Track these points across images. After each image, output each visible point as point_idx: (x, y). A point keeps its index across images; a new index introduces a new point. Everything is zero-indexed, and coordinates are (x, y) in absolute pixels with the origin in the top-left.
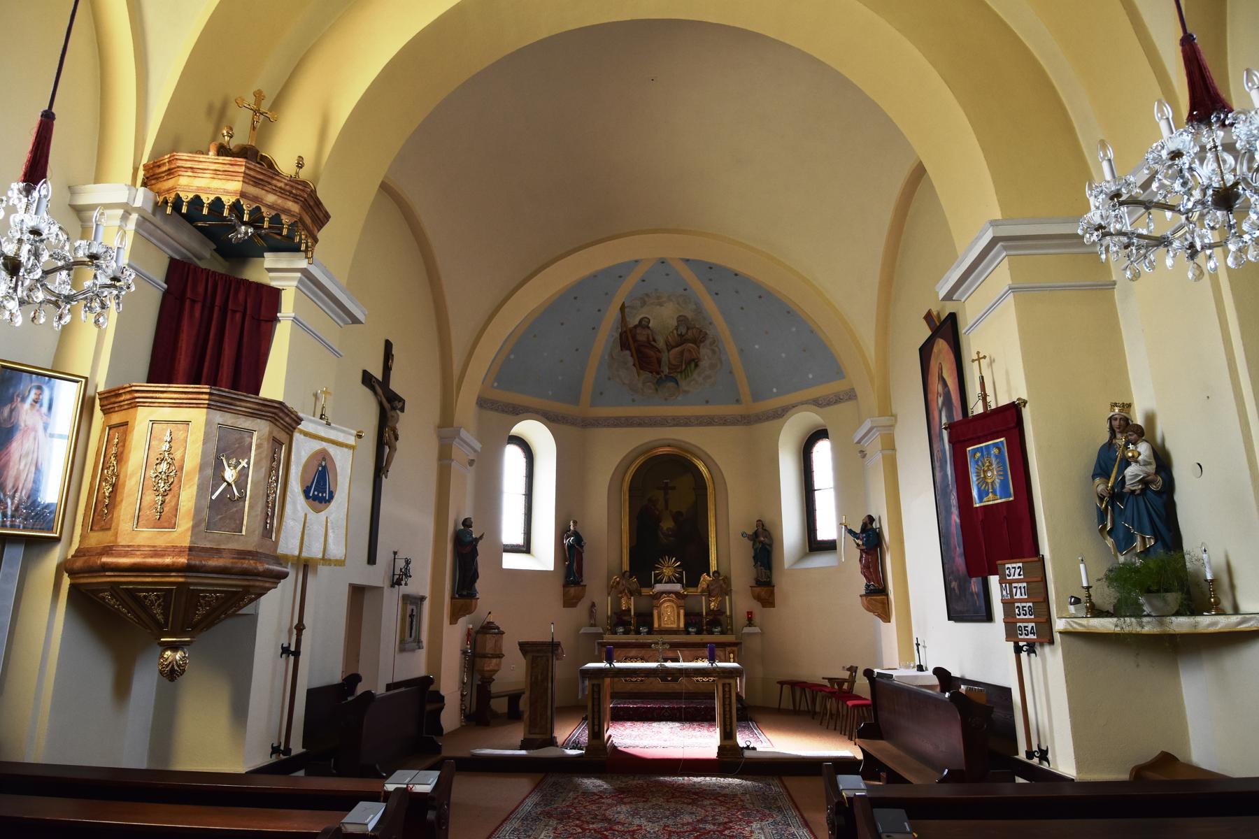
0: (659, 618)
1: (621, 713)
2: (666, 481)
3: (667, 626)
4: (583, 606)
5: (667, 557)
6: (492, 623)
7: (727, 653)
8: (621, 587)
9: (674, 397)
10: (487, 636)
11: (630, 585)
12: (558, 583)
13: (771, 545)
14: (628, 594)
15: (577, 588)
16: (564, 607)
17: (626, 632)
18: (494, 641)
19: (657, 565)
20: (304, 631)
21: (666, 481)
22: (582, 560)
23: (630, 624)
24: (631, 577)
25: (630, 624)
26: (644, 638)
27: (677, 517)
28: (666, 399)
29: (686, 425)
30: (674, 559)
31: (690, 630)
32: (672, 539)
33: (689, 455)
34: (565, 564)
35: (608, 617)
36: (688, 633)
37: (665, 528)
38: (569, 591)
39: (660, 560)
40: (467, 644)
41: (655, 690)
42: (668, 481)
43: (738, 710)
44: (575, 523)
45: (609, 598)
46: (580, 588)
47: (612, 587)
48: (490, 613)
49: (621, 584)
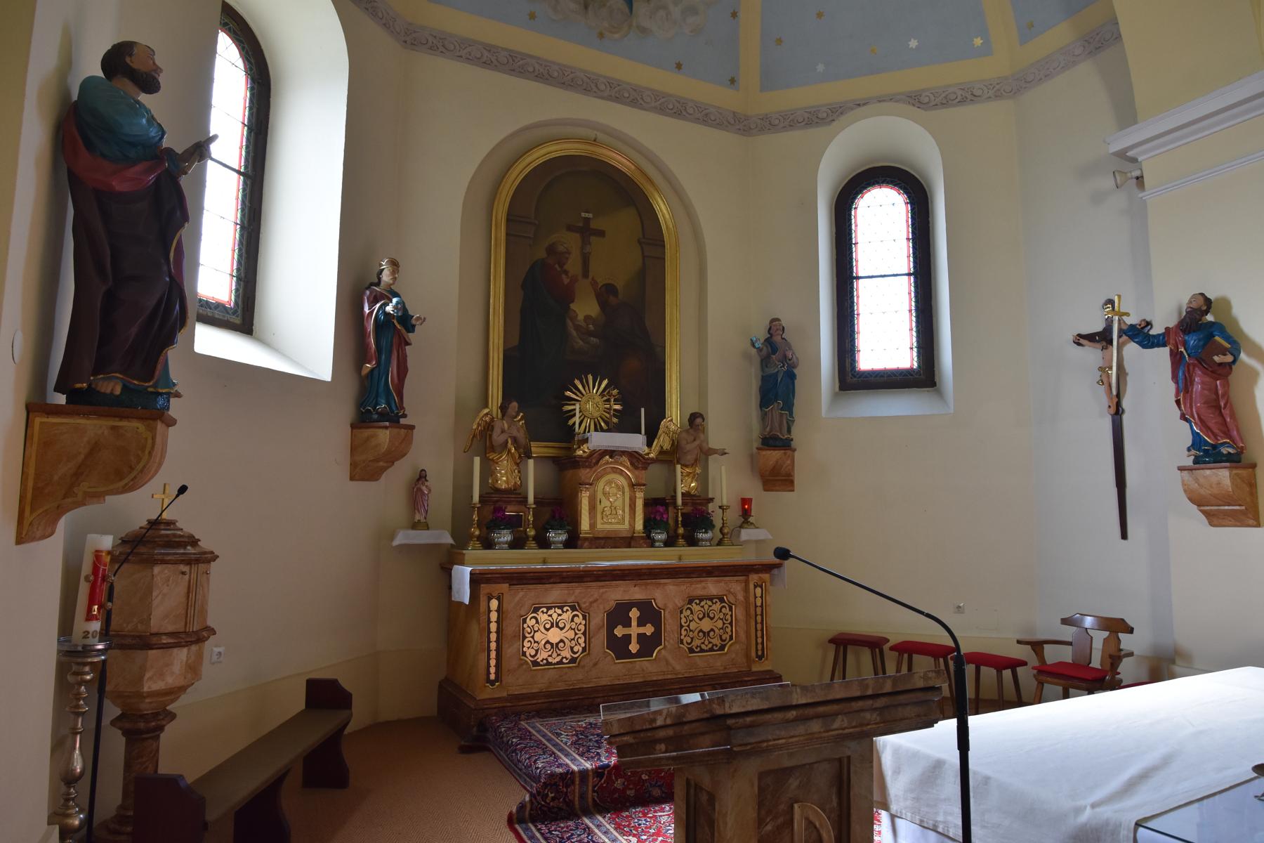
0: (593, 508)
1: (619, 784)
2: (587, 215)
3: (608, 527)
4: (397, 477)
5: (590, 377)
6: (170, 523)
7: (752, 586)
9: (617, 36)
10: (157, 569)
12: (344, 411)
16: (352, 479)
17: (517, 544)
18: (182, 589)
19: (568, 393)
20: (1190, 443)
21: (587, 215)
26: (560, 559)
27: (605, 294)
28: (601, 36)
30: (605, 382)
31: (551, 534)
36: (652, 543)
37: (581, 317)
38: (368, 439)
39: (577, 382)
40: (89, 617)
41: (605, 681)
42: (590, 216)
44: (394, 264)
48: (183, 490)
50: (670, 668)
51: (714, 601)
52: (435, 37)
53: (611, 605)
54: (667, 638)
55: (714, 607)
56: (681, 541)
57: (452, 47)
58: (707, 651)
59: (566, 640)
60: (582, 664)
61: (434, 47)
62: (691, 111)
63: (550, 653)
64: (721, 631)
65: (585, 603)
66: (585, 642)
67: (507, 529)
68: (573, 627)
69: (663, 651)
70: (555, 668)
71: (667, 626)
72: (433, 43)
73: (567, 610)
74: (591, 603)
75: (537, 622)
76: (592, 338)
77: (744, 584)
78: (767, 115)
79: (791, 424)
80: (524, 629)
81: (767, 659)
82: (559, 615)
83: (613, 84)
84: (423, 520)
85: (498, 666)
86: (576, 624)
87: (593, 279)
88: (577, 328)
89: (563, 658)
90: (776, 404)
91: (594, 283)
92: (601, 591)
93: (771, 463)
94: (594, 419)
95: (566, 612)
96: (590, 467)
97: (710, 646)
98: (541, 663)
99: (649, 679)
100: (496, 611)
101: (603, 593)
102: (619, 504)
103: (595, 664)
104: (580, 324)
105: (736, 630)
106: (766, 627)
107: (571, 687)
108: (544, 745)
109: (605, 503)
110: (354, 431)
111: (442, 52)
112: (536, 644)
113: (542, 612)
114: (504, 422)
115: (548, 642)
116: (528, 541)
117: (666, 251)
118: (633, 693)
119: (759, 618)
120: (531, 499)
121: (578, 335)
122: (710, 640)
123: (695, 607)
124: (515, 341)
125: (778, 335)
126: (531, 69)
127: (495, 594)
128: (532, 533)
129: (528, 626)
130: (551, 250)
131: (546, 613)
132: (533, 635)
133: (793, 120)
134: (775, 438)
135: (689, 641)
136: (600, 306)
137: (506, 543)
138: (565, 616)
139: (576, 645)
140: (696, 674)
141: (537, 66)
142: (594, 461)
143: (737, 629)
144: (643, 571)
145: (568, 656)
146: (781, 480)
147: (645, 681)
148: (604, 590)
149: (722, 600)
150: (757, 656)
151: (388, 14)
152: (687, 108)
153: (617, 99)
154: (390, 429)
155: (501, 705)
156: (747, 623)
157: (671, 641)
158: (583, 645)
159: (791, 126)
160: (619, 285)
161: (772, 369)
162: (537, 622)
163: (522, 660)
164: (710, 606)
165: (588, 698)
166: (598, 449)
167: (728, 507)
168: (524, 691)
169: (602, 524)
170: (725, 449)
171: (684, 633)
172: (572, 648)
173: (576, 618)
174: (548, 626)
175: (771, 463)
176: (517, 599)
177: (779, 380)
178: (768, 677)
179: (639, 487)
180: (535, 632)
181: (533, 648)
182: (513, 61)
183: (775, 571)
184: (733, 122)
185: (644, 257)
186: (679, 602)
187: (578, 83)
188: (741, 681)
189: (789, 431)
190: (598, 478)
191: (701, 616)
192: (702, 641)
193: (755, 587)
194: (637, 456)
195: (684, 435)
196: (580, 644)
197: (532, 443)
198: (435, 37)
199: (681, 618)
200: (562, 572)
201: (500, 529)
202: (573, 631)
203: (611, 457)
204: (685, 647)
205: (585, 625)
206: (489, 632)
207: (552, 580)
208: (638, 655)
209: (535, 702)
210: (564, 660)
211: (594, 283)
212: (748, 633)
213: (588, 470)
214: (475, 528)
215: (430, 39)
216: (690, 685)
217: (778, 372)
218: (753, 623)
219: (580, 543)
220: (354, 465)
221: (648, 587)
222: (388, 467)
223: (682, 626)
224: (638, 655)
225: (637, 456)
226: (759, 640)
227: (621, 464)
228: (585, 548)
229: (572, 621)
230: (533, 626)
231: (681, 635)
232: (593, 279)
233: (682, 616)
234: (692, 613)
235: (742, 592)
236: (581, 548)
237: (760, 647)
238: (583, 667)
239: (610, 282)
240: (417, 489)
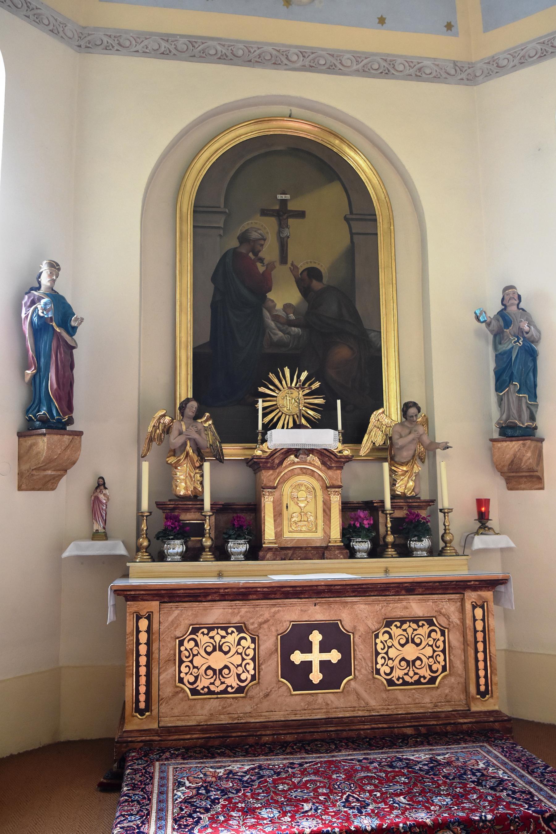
0: (278, 515)
2: (284, 197)
5: (287, 371)
7: (468, 607)
8: (175, 440)
11: (198, 432)
13: (536, 341)
14: (195, 458)
15: (56, 438)
16: (20, 489)
19: (262, 389)
21: (284, 197)
22: (72, 367)
23: (203, 536)
24: (198, 416)
25: (199, 530)
29: (331, 69)
31: (357, 546)
32: (295, 330)
33: (337, 142)
34: (23, 375)
35: (140, 516)
36: (352, 554)
37: (279, 306)
38: (31, 447)
39: (272, 376)
41: (278, 716)
42: (288, 197)
43: (551, 790)
44: (54, 267)
45: (145, 465)
46: (66, 438)
47: (151, 440)
49: (174, 432)
50: (363, 704)
51: (420, 624)
52: (110, 36)
53: (286, 627)
54: (358, 668)
55: (420, 631)
56: (391, 551)
57: (127, 43)
58: (412, 684)
59: (231, 666)
60: (250, 694)
61: (109, 46)
62: (401, 68)
63: (212, 680)
64: (431, 660)
65: (253, 624)
66: (254, 669)
67: (178, 539)
68: (240, 651)
69: (352, 683)
70: (217, 698)
71: (357, 652)
72: (108, 43)
73: (233, 632)
74: (260, 624)
75: (197, 645)
76: (293, 328)
77: (459, 604)
78: (493, 57)
79: (533, 409)
80: (180, 652)
81: (492, 696)
82: (223, 637)
83: (306, 52)
84: (101, 530)
85: (148, 693)
86: (244, 648)
87: (292, 264)
88: (276, 318)
89: (228, 686)
90: (512, 387)
91: (294, 268)
92: (273, 610)
93: (508, 456)
94: (293, 415)
95: (231, 634)
96: (273, 468)
97: (416, 677)
98: (201, 691)
99: (333, 716)
100: (146, 631)
101: (275, 613)
102: (311, 508)
103: (267, 695)
104: (280, 314)
105: (450, 659)
106: (490, 656)
107: (236, 721)
108: (150, 800)
109: (293, 508)
110: (20, 439)
111: (117, 50)
112: (196, 670)
113: (203, 633)
114: (183, 423)
115: (209, 668)
116: (388, 548)
117: (378, 224)
118: (310, 732)
119: (480, 646)
120: (207, 505)
121: (276, 326)
122: (416, 671)
123: (394, 631)
124: (206, 338)
125: (512, 304)
126: (212, 52)
127: (143, 613)
128: (207, 542)
129: (186, 649)
130: (244, 238)
131: (207, 634)
132: (192, 660)
133: (524, 56)
134: (514, 427)
135: (388, 671)
136: (300, 292)
137: (177, 554)
138: (230, 638)
139: (244, 672)
140: (395, 712)
141: (219, 48)
142: (277, 461)
143: (452, 657)
144: (320, 588)
145: (235, 685)
146: (526, 477)
147: (329, 718)
148: (277, 609)
149: (430, 623)
150: (479, 692)
151: (56, 20)
152: (396, 64)
153: (312, 68)
154: (47, 436)
155: (148, 738)
156: (465, 651)
157: (363, 671)
158: (252, 672)
159: (521, 63)
160: (324, 267)
161: (506, 345)
162: (197, 645)
163: (178, 687)
164: (414, 630)
165: (253, 736)
166: (279, 448)
167: (451, 510)
168: (179, 723)
169: (290, 532)
170: (447, 443)
171: (380, 661)
172: (238, 676)
173: (243, 642)
174: (209, 649)
175: (508, 456)
176: (171, 619)
177: (513, 359)
178: (492, 719)
179: (334, 490)
180: (194, 656)
181: (191, 674)
182: (193, 46)
183: (501, 588)
184: (453, 72)
185: (352, 234)
186: (373, 624)
187: (267, 58)
188: (454, 723)
189: (532, 418)
190: (284, 480)
191: (403, 641)
192: (406, 671)
193: (474, 607)
194: (328, 454)
195: (398, 428)
196: (248, 672)
197: (223, 445)
198: (110, 36)
199: (376, 644)
200: (219, 589)
201: (169, 539)
202: (240, 656)
203: (296, 456)
204: (382, 679)
205: (254, 649)
206: (138, 655)
207: (210, 598)
208: (321, 685)
209: (189, 736)
210: (229, 689)
211: (294, 268)
212: (465, 663)
213: (271, 472)
214: (143, 538)
215: (105, 39)
216: (385, 726)
217: (512, 347)
218: (471, 652)
219: (261, 554)
220: (21, 475)
221: (333, 606)
222: (62, 476)
223: (377, 654)
224: (321, 685)
225: (328, 454)
226: (482, 673)
227: (310, 464)
228: (268, 560)
229: (239, 644)
230: (191, 649)
231: (377, 663)
232: (292, 264)
233: (378, 641)
234: (391, 637)
235: (457, 614)
236: (263, 559)
237: (482, 681)
238: (252, 698)
239: (309, 266)
240: (95, 497)
